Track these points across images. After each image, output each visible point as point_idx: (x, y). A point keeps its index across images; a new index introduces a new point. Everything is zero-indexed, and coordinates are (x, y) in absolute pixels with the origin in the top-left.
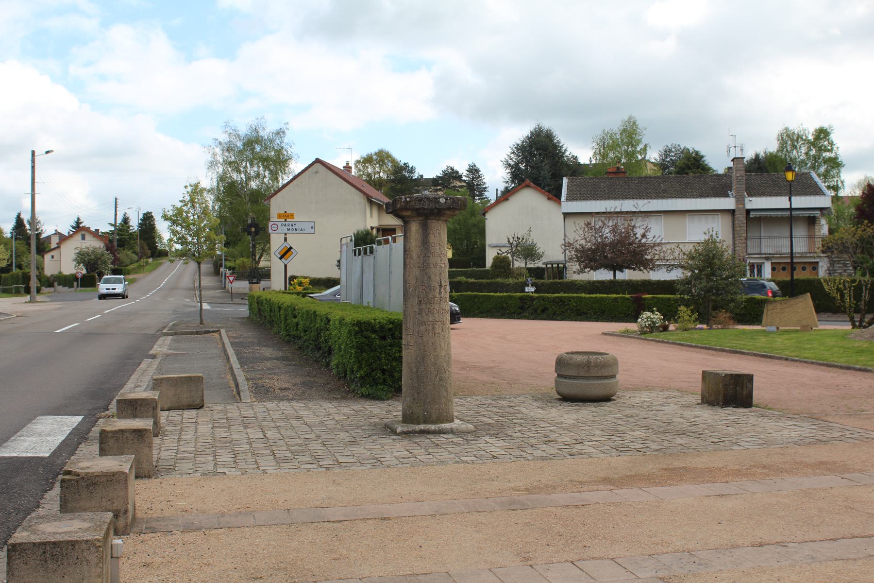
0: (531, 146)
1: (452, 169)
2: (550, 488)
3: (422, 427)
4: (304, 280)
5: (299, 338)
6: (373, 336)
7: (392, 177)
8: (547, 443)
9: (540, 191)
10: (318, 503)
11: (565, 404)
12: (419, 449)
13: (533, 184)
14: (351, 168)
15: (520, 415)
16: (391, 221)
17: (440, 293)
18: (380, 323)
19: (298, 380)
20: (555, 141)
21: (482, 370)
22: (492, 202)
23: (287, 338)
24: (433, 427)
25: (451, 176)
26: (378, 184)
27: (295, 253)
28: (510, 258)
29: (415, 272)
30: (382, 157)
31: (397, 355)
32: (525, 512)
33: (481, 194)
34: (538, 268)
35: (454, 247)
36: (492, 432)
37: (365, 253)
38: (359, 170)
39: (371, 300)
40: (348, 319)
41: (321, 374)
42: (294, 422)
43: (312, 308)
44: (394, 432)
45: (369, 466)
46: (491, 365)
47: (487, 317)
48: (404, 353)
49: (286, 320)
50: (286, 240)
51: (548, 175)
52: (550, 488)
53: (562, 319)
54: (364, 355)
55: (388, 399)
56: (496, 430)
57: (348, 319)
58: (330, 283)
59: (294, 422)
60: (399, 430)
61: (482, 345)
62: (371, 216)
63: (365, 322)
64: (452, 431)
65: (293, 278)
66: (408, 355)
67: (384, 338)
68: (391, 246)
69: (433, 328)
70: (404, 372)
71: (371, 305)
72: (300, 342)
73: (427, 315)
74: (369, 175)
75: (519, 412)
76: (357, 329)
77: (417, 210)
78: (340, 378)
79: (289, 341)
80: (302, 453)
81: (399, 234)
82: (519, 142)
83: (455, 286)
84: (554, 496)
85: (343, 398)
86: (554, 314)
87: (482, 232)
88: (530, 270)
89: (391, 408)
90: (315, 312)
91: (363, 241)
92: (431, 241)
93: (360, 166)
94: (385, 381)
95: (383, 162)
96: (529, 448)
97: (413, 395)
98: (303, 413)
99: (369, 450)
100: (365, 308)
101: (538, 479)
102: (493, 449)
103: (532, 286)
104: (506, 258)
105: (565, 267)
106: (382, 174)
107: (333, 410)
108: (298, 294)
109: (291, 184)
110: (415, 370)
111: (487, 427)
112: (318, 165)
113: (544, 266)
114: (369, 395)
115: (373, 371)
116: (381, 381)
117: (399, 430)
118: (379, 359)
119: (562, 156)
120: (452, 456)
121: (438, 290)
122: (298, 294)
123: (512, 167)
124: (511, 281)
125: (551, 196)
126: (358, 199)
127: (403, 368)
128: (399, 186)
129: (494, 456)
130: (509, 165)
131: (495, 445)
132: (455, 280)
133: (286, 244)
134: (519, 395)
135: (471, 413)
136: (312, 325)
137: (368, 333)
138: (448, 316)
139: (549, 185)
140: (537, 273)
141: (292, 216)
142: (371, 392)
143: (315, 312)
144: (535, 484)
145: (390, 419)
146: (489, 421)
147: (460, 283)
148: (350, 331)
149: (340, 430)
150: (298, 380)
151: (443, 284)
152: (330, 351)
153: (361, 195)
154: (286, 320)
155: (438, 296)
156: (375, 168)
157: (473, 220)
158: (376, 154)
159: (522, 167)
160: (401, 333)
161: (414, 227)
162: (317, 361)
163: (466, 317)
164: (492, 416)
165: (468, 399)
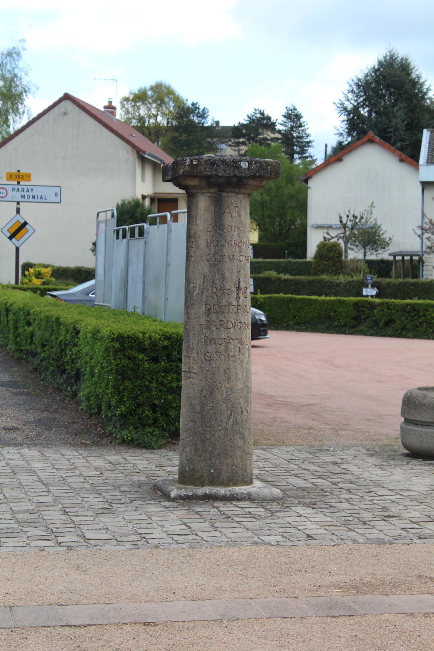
0: (377, 81)
1: (262, 114)
2: (388, 587)
3: (207, 490)
4: (43, 270)
5: (35, 355)
6: (141, 357)
7: (175, 123)
8: (386, 518)
9: (389, 149)
10: (54, 599)
11: (414, 462)
12: (201, 522)
13: (378, 139)
14: (114, 108)
15: (348, 477)
16: (170, 189)
17: (238, 298)
18: (150, 338)
19: (31, 417)
20: (414, 76)
21: (297, 408)
22: (320, 162)
23: (17, 355)
24: (222, 491)
25: (260, 124)
26: (153, 133)
27: (31, 231)
28: (343, 245)
29: (203, 267)
30: (161, 94)
31: (174, 385)
32: (352, 620)
33: (303, 151)
34: (382, 261)
35: (262, 228)
36: (307, 501)
37: (132, 235)
38: (127, 112)
39: (139, 303)
40: (105, 332)
41: (64, 408)
42: (24, 478)
43: (54, 312)
44: (166, 496)
45: (129, 546)
46: (310, 401)
47: (306, 330)
48: (184, 383)
49: (16, 328)
50: (18, 211)
51: (402, 125)
52: (388, 587)
53: (415, 337)
54: (127, 383)
55: (159, 448)
56: (313, 498)
57: (105, 332)
58: (83, 275)
59: (24, 478)
60: (174, 493)
61: (299, 373)
62: (143, 180)
63: (128, 337)
64: (249, 498)
65: (27, 266)
66: (190, 386)
67: (155, 360)
68: (169, 227)
69: (227, 349)
70: (184, 411)
71: (139, 311)
72: (36, 361)
73: (218, 329)
74: (141, 119)
75: (348, 472)
76: (117, 345)
77: (207, 178)
78: (91, 415)
79: (19, 359)
80: (33, 523)
81: (182, 208)
82: (361, 76)
83: (261, 285)
84: (394, 599)
85: (96, 444)
86: (404, 328)
87: (303, 207)
88: (370, 263)
89: (163, 461)
90: (58, 319)
91: (130, 217)
92: (227, 223)
93: (128, 106)
94: (155, 421)
95: (162, 101)
96: (360, 525)
97: (195, 444)
98: (36, 465)
99: (129, 521)
100: (129, 315)
101: (371, 571)
102: (308, 525)
103: (373, 286)
104: (335, 246)
105: (421, 261)
106: (159, 118)
107: (80, 462)
108: (34, 290)
109: (46, 116)
110: (198, 408)
111: (300, 493)
112: (67, 104)
113: (391, 258)
114: (132, 440)
115: (139, 406)
116: (150, 422)
117: (174, 493)
118: (149, 390)
119: (423, 98)
120: (249, 534)
121: (234, 295)
122: (34, 290)
123: (349, 113)
124: (342, 279)
125: (404, 156)
126: (125, 154)
127: (183, 404)
128: (184, 137)
129: (308, 536)
130: (345, 109)
131: (312, 520)
132: (262, 275)
133: (18, 217)
134: (348, 448)
135: (278, 471)
136: (53, 337)
137: (134, 353)
138: (248, 332)
139: (402, 140)
140: (381, 268)
141: (28, 177)
142: (135, 436)
143: (58, 319)
144: (367, 579)
145: (161, 476)
146: (301, 483)
147: (268, 280)
148: (107, 349)
149: (89, 491)
150: (31, 417)
151: (242, 285)
152: (78, 376)
153: (129, 148)
154: (16, 328)
155: (234, 303)
156: (150, 110)
157: (289, 190)
158: (152, 88)
159: (364, 112)
160: (180, 353)
161: (203, 203)
162: (59, 390)
163: (277, 329)
164: (309, 476)
165: (275, 451)
